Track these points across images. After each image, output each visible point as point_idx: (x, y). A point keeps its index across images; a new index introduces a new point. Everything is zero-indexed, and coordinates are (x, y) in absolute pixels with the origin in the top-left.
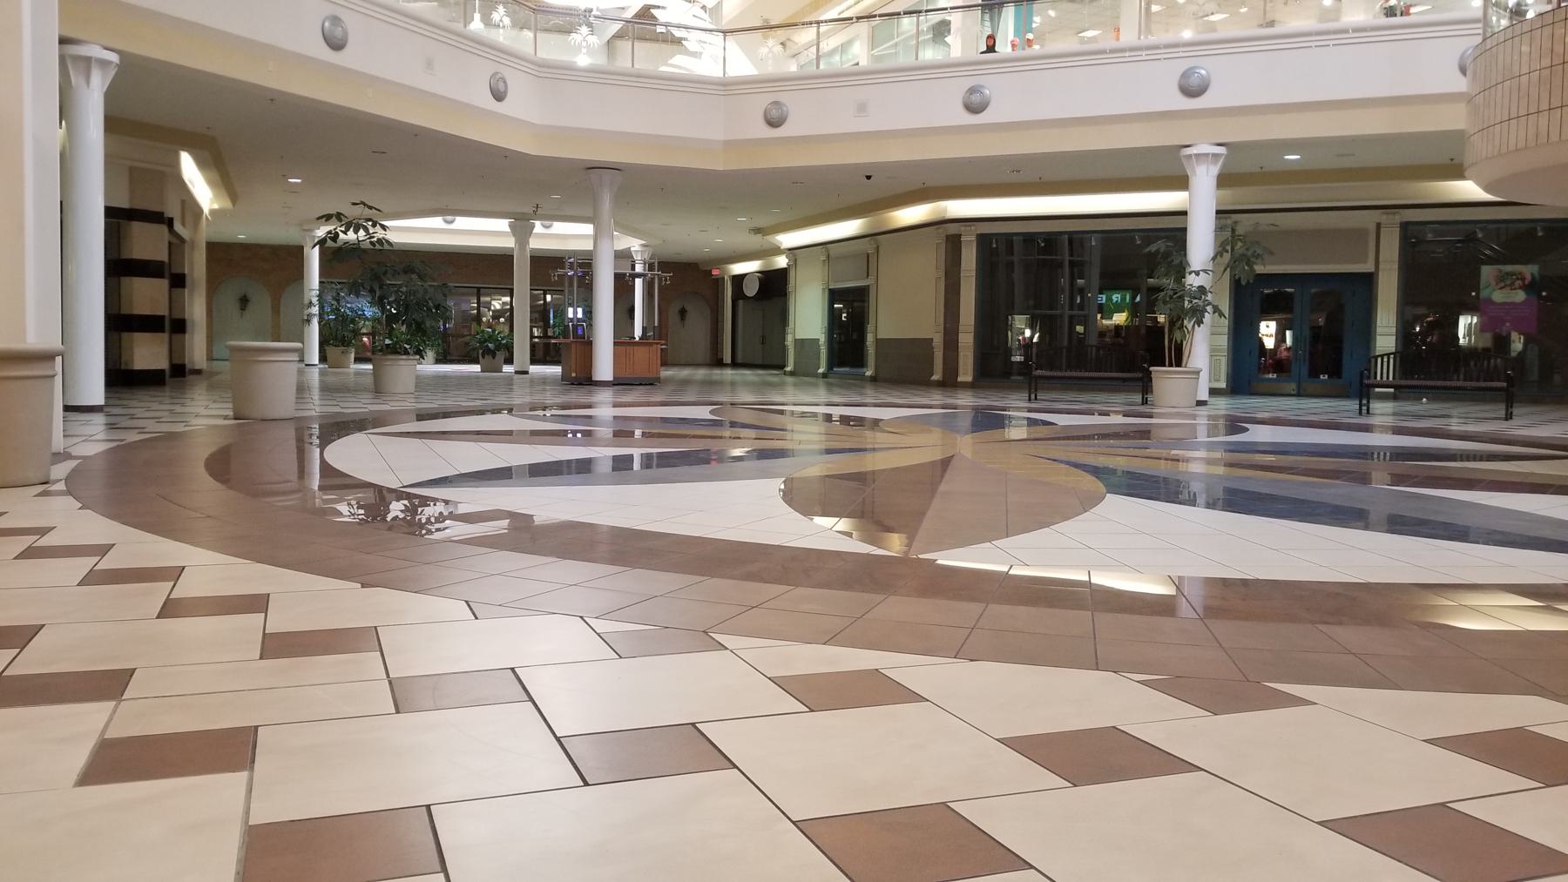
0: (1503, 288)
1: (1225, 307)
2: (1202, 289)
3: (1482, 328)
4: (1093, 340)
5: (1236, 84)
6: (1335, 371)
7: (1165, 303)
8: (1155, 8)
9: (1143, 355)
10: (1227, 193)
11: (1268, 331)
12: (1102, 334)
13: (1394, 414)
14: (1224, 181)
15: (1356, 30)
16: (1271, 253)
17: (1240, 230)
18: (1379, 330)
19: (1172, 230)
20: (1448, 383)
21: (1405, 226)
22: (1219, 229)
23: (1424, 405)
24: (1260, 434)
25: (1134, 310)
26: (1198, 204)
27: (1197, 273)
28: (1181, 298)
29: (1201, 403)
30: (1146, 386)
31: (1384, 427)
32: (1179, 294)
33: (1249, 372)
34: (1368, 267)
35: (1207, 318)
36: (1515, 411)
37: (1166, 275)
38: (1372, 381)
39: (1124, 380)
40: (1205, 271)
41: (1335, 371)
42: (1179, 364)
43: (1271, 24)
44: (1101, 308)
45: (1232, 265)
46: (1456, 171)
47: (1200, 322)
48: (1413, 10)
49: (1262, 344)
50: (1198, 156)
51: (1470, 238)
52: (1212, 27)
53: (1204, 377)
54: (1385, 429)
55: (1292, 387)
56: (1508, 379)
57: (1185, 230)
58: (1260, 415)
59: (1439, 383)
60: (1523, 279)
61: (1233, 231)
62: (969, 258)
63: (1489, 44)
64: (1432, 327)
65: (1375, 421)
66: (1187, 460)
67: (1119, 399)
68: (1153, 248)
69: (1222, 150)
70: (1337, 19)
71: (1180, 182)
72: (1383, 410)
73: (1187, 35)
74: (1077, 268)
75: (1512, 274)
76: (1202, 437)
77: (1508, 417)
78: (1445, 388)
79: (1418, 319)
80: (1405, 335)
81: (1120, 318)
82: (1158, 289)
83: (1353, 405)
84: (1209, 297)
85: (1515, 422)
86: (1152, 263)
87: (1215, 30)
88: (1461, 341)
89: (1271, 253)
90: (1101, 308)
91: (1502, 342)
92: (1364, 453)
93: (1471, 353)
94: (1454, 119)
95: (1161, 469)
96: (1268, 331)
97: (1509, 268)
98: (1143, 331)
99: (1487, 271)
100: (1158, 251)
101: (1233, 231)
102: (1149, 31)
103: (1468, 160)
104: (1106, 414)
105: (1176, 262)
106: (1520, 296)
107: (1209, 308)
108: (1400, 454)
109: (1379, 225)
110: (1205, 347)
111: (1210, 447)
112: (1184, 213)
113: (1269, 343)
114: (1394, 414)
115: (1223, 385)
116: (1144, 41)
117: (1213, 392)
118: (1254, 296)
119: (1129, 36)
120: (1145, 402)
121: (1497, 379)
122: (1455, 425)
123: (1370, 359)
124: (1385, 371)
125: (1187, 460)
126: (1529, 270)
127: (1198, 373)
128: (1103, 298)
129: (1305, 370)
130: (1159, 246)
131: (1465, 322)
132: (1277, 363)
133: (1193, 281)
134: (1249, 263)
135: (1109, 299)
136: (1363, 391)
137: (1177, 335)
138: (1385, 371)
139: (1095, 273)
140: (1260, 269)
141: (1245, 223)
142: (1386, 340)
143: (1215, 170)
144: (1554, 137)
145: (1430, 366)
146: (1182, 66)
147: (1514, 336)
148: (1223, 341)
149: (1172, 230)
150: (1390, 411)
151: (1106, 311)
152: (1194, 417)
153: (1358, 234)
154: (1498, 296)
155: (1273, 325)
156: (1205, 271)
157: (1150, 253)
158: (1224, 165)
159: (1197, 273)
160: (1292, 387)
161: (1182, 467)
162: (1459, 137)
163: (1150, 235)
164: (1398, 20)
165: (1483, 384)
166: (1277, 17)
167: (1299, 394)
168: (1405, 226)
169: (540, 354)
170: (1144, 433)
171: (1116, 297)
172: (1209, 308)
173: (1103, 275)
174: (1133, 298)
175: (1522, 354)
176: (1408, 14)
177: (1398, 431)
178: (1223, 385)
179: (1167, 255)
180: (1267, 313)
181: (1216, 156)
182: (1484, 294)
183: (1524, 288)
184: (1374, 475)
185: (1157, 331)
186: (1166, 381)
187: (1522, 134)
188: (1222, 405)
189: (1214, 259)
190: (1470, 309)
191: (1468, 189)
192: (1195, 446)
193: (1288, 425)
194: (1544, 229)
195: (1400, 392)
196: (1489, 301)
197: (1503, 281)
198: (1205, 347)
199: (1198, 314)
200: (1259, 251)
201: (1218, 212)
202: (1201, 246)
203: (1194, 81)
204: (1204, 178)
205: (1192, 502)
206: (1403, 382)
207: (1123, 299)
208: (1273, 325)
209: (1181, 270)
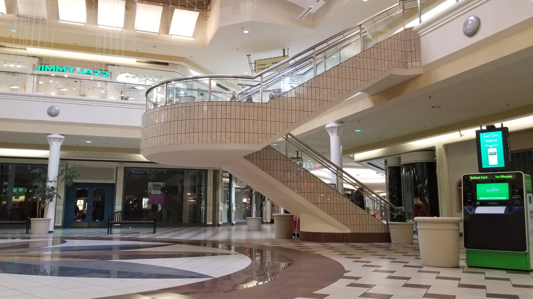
0: (154, 189)
1: (62, 194)
2: (53, 188)
3: (149, 203)
4: (10, 207)
5: (69, 114)
6: (101, 219)
7: (38, 193)
8: (40, 82)
9: (32, 211)
10: (62, 152)
11: (80, 204)
12: (15, 204)
13: (120, 233)
14: (63, 148)
15: (110, 102)
16: (79, 176)
17: (69, 167)
18: (116, 204)
19: (42, 166)
20: (140, 222)
21: (125, 168)
22: (60, 166)
23: (130, 229)
24: (70, 243)
25: (28, 195)
26: (53, 156)
27: (51, 182)
28: (45, 191)
29: (50, 232)
30: (28, 226)
31: (117, 238)
32: (44, 189)
33: (71, 219)
34: (113, 182)
35: (54, 199)
36: (157, 230)
37: (39, 182)
38: (113, 222)
39: (19, 224)
40: (54, 181)
41: (101, 219)
42: (42, 217)
43: (84, 95)
44: (14, 194)
45: (66, 178)
46: (138, 151)
47: (51, 201)
48: (130, 99)
49: (78, 208)
50: (54, 138)
51: (146, 173)
52: (63, 93)
53: (52, 222)
54: (117, 239)
55: (86, 224)
56: (155, 220)
57: (47, 165)
58: (75, 236)
59: (135, 222)
60: (160, 187)
61: (67, 167)
62: (425, 167)
63: (149, 112)
64: (135, 202)
65: (114, 236)
66: (43, 256)
67: (18, 232)
68: (34, 171)
69: (63, 137)
70: (106, 98)
71: (46, 147)
72: (117, 232)
73: (53, 94)
74: (5, 178)
75: (157, 185)
76: (50, 246)
77: (155, 232)
78: (139, 223)
79: (130, 199)
80: (125, 205)
81: (22, 198)
82: (36, 187)
83: (106, 230)
84: (56, 191)
85: (157, 234)
86: (35, 176)
87: (64, 94)
88: (143, 207)
89: (79, 176)
90: (14, 194)
91: (155, 207)
92: (109, 248)
93: (146, 211)
94: (137, 135)
95: (33, 261)
96: (80, 204)
97: (156, 183)
98: (32, 203)
99: (150, 184)
100: (36, 173)
101: (67, 167)
102: (38, 90)
103: (141, 148)
104: (14, 238)
105: (43, 177)
106: (159, 192)
107: (55, 195)
108: (122, 247)
109: (117, 167)
110: (53, 211)
111: (53, 250)
112: (47, 159)
113: (81, 208)
114: (120, 233)
115: (60, 224)
116: (35, 93)
117: (56, 227)
118: (73, 191)
119: (29, 91)
120: (27, 233)
121: (154, 220)
122: (141, 237)
123: (113, 214)
124: (118, 218)
125: (43, 256)
126: (162, 184)
127: (49, 220)
128: (15, 190)
129: (91, 218)
130: (37, 171)
131: (145, 201)
132: (82, 215)
133: (49, 185)
134: (71, 179)
135: (18, 191)
136: (110, 226)
137: (42, 206)
138: (118, 218)
139: (12, 180)
140: (75, 181)
141: (71, 164)
142: (118, 207)
143: (60, 144)
144: (165, 144)
145: (133, 216)
146: (49, 105)
147: (159, 205)
148: (61, 208)
149: (42, 166)
150: (119, 232)
151: (17, 196)
152: (47, 238)
153: (110, 170)
154: (153, 192)
155: (82, 201)
156: (54, 181)
157: (33, 173)
158: (64, 142)
159: (51, 182)
160: (86, 224)
161: (41, 259)
162: (138, 141)
163: (34, 166)
164: (124, 101)
165: (147, 222)
166: (86, 93)
167: (89, 227)
168: (125, 168)
169: (200, 176)
170: (26, 246)
171: (21, 190)
172: (55, 195)
173: (16, 181)
174: (28, 190)
175: (161, 210)
176: (128, 100)
177: (122, 239)
178: (60, 224)
179: (40, 174)
180: (79, 196)
181: (60, 139)
182: (149, 191)
183: (161, 190)
184: (113, 256)
185: (35, 203)
186: (37, 224)
187: (156, 142)
188: (59, 233)
189: (58, 177)
190: (146, 196)
191: (141, 157)
192: (47, 250)
193: (83, 239)
194: (167, 171)
195: (122, 225)
196: (151, 194)
197: (155, 187)
198: (53, 211)
199: (51, 197)
200: (75, 174)
201: (60, 159)
202: (53, 172)
203: (53, 111)
204: (56, 146)
205: (46, 274)
206: (123, 222)
207: (24, 191)
208: (82, 201)
209: (45, 180)
